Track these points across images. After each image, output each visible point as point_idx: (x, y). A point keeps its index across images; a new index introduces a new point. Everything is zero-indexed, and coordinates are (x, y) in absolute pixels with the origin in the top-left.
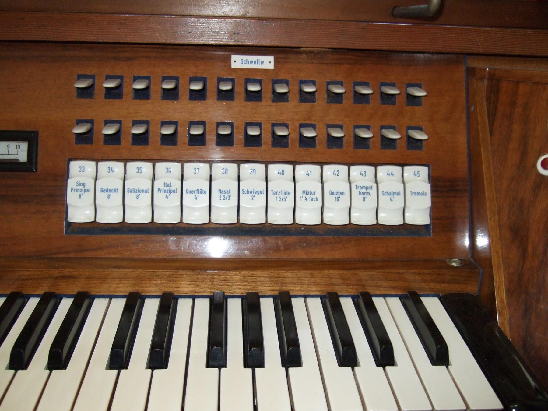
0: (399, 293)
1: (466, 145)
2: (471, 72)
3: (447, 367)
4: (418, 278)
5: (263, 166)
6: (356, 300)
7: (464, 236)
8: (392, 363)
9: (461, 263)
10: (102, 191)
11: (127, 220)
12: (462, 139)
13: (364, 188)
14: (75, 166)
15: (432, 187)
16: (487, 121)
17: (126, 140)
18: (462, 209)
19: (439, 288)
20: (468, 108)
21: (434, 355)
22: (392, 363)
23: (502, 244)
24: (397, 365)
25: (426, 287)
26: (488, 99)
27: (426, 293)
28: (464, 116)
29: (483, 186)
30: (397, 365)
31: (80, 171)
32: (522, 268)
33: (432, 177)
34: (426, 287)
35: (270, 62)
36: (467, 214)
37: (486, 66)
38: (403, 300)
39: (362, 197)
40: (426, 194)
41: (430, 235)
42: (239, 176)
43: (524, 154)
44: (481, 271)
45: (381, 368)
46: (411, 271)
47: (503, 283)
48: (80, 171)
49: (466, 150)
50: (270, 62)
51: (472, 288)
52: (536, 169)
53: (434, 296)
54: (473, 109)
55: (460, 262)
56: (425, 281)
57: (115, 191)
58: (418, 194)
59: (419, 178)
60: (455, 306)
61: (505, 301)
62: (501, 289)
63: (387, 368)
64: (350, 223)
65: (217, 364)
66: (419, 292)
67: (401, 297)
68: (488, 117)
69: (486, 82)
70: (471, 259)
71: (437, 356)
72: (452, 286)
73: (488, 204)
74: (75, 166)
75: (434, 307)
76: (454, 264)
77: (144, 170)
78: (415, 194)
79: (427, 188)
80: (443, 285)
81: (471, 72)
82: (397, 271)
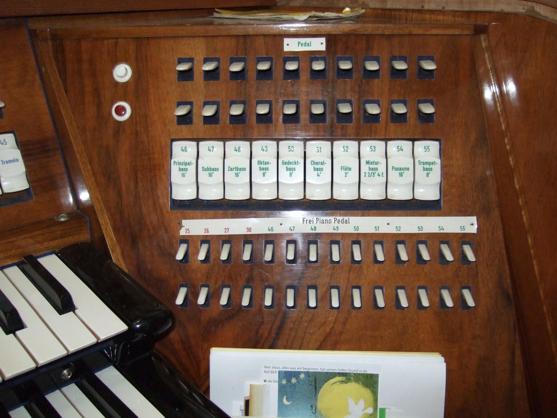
0: (16, 261)
1: (46, 106)
2: (33, 34)
3: (74, 313)
4: (31, 241)
5: (194, 143)
6: (21, 267)
7: (67, 190)
8: (21, 326)
9: (69, 217)
10: (283, 163)
11: (227, 198)
12: (41, 101)
13: (430, 164)
14: (177, 146)
15: (22, 152)
16: (60, 80)
17: (197, 121)
18: (57, 167)
19: (53, 245)
20: (40, 71)
21: (60, 307)
22: (21, 326)
23: (99, 190)
24: (26, 327)
25: (41, 247)
26: (56, 59)
27: (42, 253)
28: (37, 77)
29: (70, 142)
30: (26, 327)
31: (182, 152)
32: (121, 206)
33: (20, 142)
34: (41, 247)
35: (288, 45)
36: (63, 170)
37: (44, 27)
38: (21, 267)
39: (426, 172)
40: (17, 160)
41: (32, 198)
42: (278, 152)
43: (99, 105)
44: (88, 219)
45: (12, 335)
46: (20, 237)
47: (109, 224)
48: (182, 152)
49: (47, 111)
50: (288, 45)
51: (85, 237)
52: (112, 117)
53: (51, 253)
54: (44, 70)
55: (67, 216)
56: (39, 242)
57: (217, 169)
58: (10, 161)
59: (7, 146)
60: (71, 258)
61: (114, 239)
62: (109, 230)
63: (18, 333)
64: (413, 199)
65: (42, 370)
66: (34, 255)
67: (19, 265)
68: (60, 76)
69: (50, 43)
70: (78, 211)
71: (62, 305)
72: (66, 239)
73: (78, 156)
74: (177, 146)
75: (54, 265)
76: (62, 220)
77: (189, 149)
78: (7, 162)
79: (17, 154)
80: (56, 241)
81: (33, 34)
82: (6, 241)
